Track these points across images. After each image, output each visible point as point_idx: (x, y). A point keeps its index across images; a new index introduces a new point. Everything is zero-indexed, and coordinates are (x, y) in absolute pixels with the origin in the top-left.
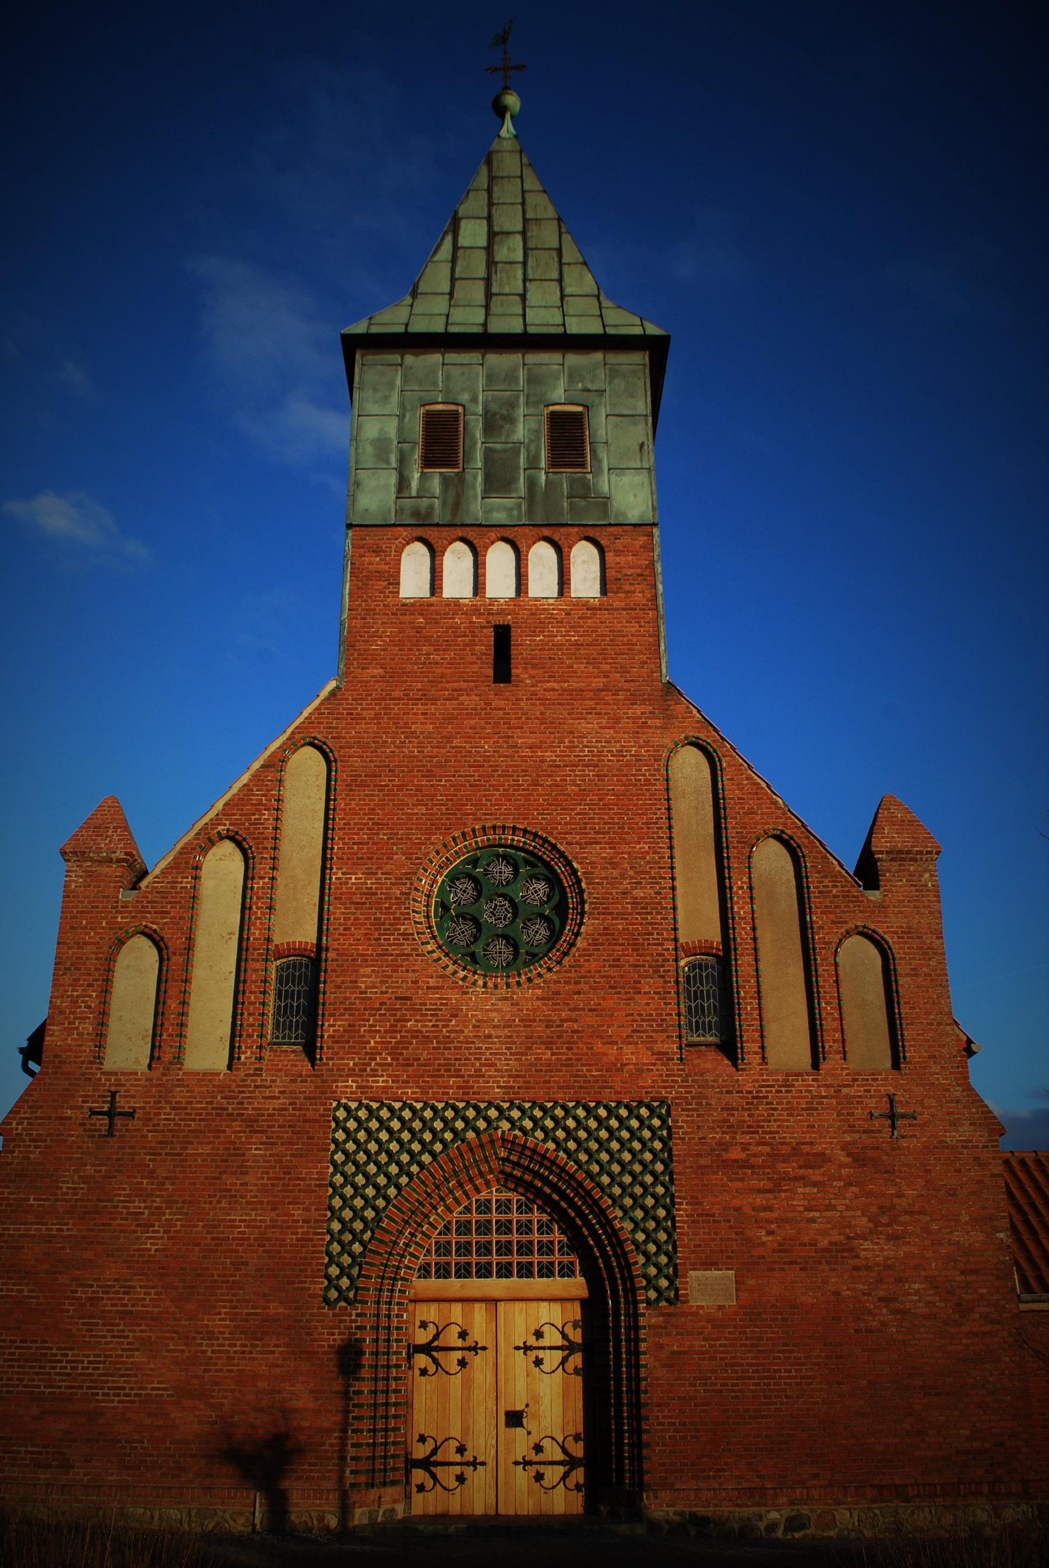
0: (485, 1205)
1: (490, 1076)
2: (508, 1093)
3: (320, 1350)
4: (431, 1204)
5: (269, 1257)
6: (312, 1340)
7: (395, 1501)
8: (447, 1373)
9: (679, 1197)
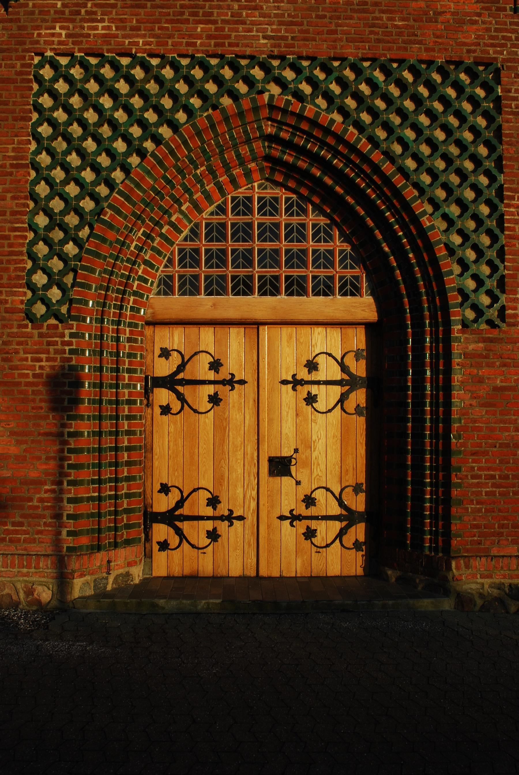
0: (244, 205)
1: (253, 23)
2: (279, 46)
3: (22, 380)
4: (172, 197)
6: (11, 368)
8: (195, 411)
9: (509, 190)
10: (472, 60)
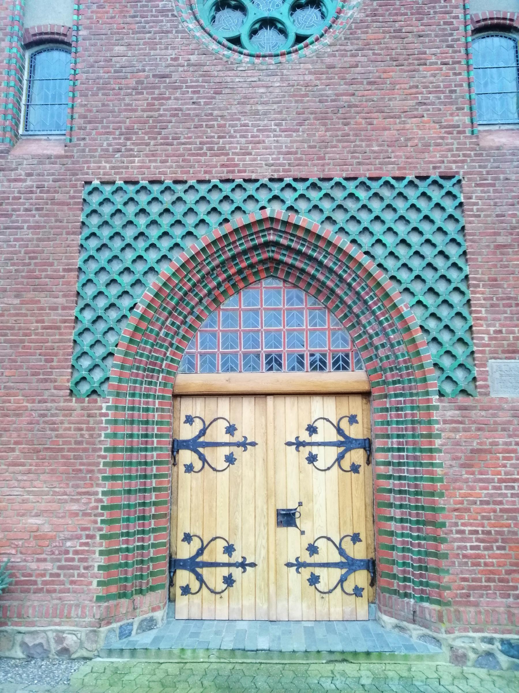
1: (257, 154)
2: (278, 171)
5: (11, 347)
7: (154, 610)
8: (214, 469)
10: (437, 174)
